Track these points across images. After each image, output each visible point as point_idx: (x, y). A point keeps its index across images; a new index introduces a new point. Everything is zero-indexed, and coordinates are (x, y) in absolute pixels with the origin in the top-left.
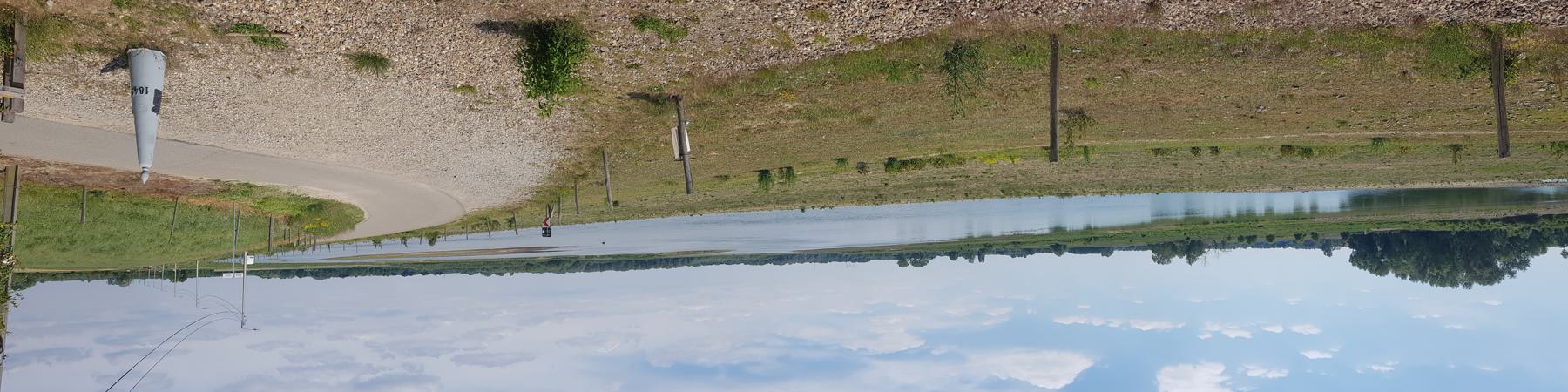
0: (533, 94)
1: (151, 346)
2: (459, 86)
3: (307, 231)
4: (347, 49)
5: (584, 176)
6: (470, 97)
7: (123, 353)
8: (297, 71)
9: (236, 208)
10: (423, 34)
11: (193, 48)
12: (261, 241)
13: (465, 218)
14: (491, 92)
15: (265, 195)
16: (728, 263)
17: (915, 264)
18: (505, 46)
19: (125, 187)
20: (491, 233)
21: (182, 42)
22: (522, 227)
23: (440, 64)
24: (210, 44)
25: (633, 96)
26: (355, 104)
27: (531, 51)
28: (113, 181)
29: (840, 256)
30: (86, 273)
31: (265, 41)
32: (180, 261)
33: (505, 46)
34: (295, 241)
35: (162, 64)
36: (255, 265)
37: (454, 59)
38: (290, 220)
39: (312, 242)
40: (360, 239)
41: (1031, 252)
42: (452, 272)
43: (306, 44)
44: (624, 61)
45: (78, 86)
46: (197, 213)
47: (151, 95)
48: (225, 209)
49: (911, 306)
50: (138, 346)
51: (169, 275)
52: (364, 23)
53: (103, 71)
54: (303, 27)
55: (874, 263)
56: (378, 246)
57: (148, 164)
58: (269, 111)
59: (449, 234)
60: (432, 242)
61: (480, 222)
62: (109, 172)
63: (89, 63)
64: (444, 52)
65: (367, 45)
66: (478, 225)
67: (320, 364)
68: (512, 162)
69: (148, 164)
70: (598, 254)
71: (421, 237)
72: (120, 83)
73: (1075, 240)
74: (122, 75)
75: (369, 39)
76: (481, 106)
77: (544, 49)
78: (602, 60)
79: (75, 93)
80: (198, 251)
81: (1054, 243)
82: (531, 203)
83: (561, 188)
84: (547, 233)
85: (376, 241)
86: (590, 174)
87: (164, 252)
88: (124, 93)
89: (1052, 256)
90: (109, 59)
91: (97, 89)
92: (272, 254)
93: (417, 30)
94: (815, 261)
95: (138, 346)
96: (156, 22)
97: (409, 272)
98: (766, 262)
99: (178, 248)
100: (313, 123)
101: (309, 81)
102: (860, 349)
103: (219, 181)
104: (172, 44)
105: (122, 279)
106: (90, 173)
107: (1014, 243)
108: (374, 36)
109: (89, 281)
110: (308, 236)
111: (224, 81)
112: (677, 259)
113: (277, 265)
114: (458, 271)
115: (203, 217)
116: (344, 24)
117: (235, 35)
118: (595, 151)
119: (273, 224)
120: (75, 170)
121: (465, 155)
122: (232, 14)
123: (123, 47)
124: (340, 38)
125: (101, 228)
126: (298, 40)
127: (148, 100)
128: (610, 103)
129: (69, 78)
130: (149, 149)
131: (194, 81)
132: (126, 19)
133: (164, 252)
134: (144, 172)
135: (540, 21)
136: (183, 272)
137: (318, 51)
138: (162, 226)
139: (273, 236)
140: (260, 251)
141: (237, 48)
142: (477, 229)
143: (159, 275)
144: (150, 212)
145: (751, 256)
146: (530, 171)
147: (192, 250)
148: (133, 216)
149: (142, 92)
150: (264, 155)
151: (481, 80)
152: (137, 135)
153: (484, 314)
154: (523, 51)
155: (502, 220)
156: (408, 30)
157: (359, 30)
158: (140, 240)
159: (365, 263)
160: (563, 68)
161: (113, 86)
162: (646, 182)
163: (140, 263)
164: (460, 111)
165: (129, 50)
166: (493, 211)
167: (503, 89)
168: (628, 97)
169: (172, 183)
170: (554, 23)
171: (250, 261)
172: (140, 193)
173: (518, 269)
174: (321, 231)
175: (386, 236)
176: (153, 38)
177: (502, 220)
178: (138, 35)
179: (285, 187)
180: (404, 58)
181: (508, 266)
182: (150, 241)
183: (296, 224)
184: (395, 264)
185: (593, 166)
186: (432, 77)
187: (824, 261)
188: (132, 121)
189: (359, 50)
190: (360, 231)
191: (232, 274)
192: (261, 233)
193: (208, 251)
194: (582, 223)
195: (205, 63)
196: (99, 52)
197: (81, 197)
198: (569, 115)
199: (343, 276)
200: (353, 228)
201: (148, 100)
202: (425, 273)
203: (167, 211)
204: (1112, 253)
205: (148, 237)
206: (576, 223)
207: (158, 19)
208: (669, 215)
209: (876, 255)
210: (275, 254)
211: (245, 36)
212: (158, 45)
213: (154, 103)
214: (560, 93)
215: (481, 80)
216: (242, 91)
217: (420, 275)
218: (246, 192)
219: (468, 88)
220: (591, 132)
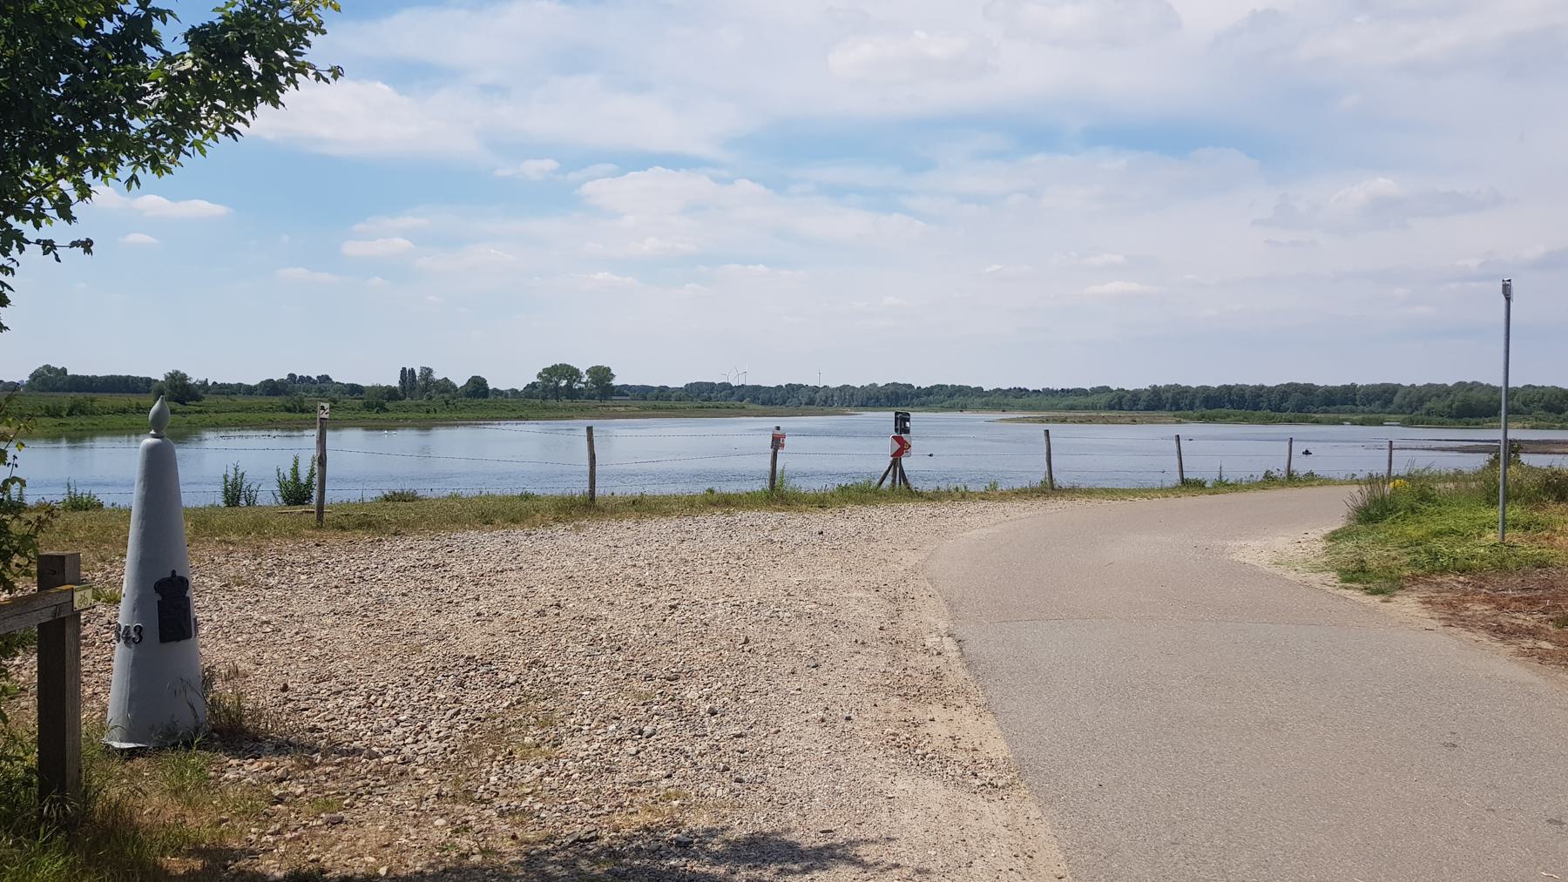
16: (1021, 392)
17: (571, 373)
29: (754, 400)
41: (271, 388)
49: (600, 276)
55: (677, 381)
70: (1347, 429)
73: (124, 411)
81: (192, 406)
89: (195, 376)
94: (816, 389)
98: (930, 391)
102: (730, 182)
107: (302, 411)
145: (963, 408)
187: (793, 389)
204: (34, 376)
209: (668, 398)
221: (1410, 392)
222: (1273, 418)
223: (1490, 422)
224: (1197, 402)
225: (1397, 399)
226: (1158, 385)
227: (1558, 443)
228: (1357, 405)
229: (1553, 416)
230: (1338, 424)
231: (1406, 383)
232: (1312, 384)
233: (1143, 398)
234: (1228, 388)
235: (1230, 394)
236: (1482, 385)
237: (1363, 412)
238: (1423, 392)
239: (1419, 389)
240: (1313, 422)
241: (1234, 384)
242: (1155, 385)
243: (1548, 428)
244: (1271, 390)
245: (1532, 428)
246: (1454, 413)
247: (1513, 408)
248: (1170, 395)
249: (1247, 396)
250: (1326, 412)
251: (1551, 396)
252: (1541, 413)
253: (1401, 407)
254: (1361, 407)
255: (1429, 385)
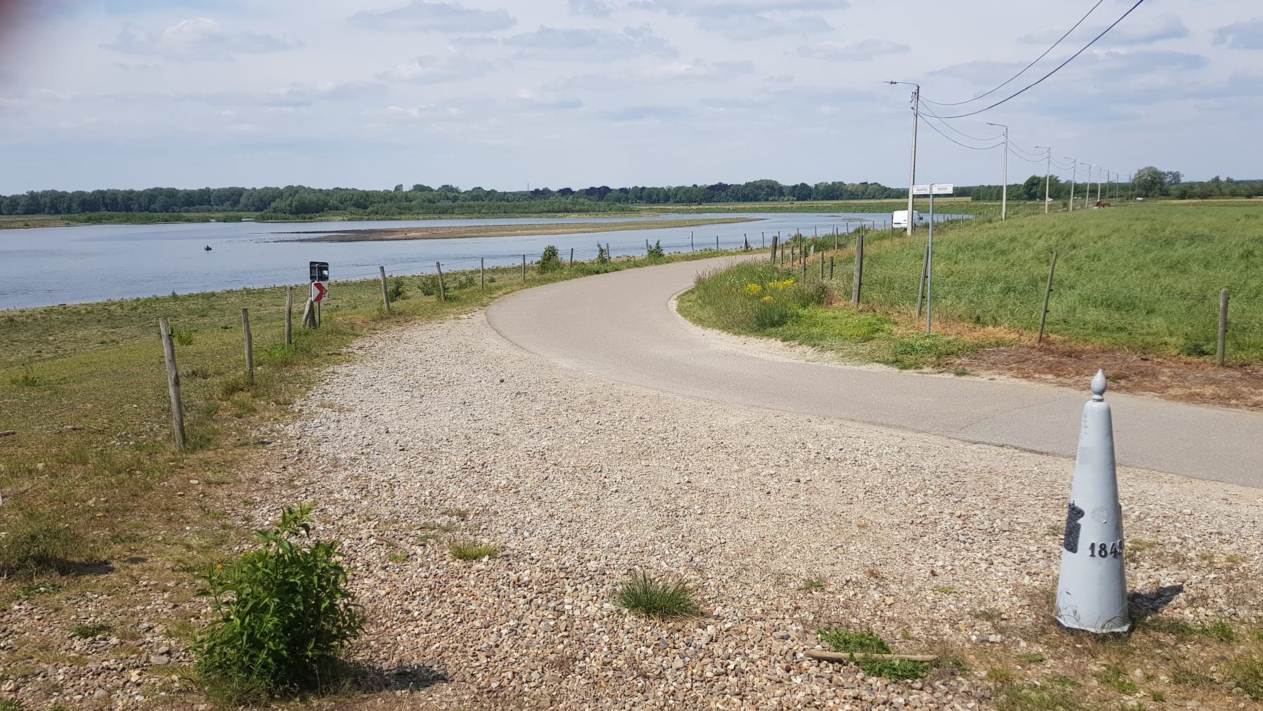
0: (321, 553)
1: (1096, 51)
2: (485, 559)
3: (788, 274)
4: (704, 628)
5: (231, 390)
6: (463, 537)
7: (1150, 39)
8: (802, 585)
9: (925, 322)
10: (552, 657)
11: (1001, 631)
12: (879, 256)
13: (485, 300)
14: (419, 551)
15: (868, 347)
18: (384, 644)
19: (1143, 364)
20: (437, 272)
21: (1023, 644)
22: (376, 282)
23: (522, 601)
24: (969, 640)
25: (103, 567)
26: (690, 520)
27: (325, 639)
28: (1165, 376)
30: (1223, 195)
31: (861, 644)
32: (1039, 218)
33: (384, 644)
34: (813, 256)
35: (1062, 601)
36: (891, 209)
37: (491, 611)
38: (821, 297)
39: (779, 253)
40: (687, 258)
42: (514, 194)
43: (782, 638)
44: (114, 640)
45: (1229, 559)
46: (1001, 312)
47: (1084, 541)
48: (946, 319)
50: (1121, 50)
51: (1060, 191)
52: (669, 677)
53: (1179, 589)
54: (788, 670)
56: (654, 245)
57: (1093, 408)
58: (857, 508)
59: (517, 269)
60: (551, 253)
61: (456, 293)
62: (1171, 391)
63: (1205, 605)
64: (511, 623)
65: (665, 634)
66: (462, 286)
67: (767, 15)
68: (386, 412)
69: (1093, 408)
70: (213, 225)
71: (572, 264)
72: (1147, 565)
74: (1141, 580)
75: (660, 647)
76: (443, 521)
77: (296, 645)
78: (169, 635)
79: (1234, 546)
80: (1002, 239)
82: (353, 332)
83: (286, 363)
84: (318, 270)
85: (656, 255)
86: (218, 393)
87: (1070, 234)
88: (1138, 546)
90: (1166, 613)
91: (1192, 554)
92: (858, 231)
93: (564, 665)
95: (1121, 50)
96: (1073, 684)
97: (596, 197)
99: (1041, 244)
100: (772, 484)
101: (778, 565)
103: (957, 374)
104: (1043, 639)
105: (1153, 183)
106: (1209, 390)
108: (650, 651)
109: (1217, 179)
110: (788, 266)
111: (943, 567)
112: (27, 212)
113: (847, 209)
114: (504, 197)
115: (991, 303)
116: (709, 674)
117: (919, 657)
118: (204, 443)
119: (855, 289)
120: (1238, 396)
121: (479, 424)
122: (925, 696)
123: (1138, 636)
124: (717, 648)
125: (1189, 283)
126: (798, 646)
127: (1091, 531)
128: (161, 546)
129: (1244, 576)
130: (1090, 438)
131: (1003, 569)
132: (1130, 689)
133: (1070, 234)
134: (1101, 393)
135: (303, 700)
136: (1032, 197)
137: (759, 624)
138: (1072, 287)
139: (855, 267)
140: (882, 237)
141: (916, 631)
142: (463, 278)
143: (1080, 190)
144: (1094, 315)
146: (350, 396)
147: (1013, 239)
148: (1127, 306)
149: (1103, 547)
150: (870, 422)
151: (440, 572)
152: (1113, 464)
153: (453, 111)
154: (345, 637)
155: (415, 297)
156: (582, 664)
157: (679, 663)
158: (1115, 260)
159: (677, 211)
160: (254, 608)
161: (1160, 560)
162: (91, 384)
163: (1115, 215)
164: (485, 509)
165: (1126, 628)
166: (431, 315)
167: (395, 558)
168: (115, 564)
169: (1050, 369)
170: (272, 698)
171: (901, 218)
172: (1112, 351)
173: (386, 197)
174: (763, 275)
175: (637, 264)
176: (1079, 653)
177: (415, 297)
178: (1108, 658)
179: (830, 362)
180: (592, 609)
181: (405, 204)
182: (1096, 257)
183: (810, 289)
184: (623, 210)
185: (211, 412)
186: (538, 575)
188: (1123, 492)
189: (679, 625)
190: (685, 276)
191: (935, 191)
192: (879, 272)
193: (980, 237)
194: (249, 292)
195: (980, 604)
196: (1186, 625)
197: (1229, 343)
198: (256, 514)
199: (721, 187)
200: (700, 281)
201: (1091, 531)
202: (566, 192)
203: (1061, 316)
205: (1099, 266)
206: (261, 292)
207: (1069, 689)
208: (49, 311)
210: (851, 230)
211: (901, 653)
212: (1068, 639)
213: (1078, 527)
214: (262, 557)
215: (440, 572)
216: (909, 547)
217: (575, 189)
218: (905, 352)
219: (467, 555)
220: (209, 483)
221: (253, 194)
222: (152, 218)
223: (320, 216)
224: (75, 206)
225: (243, 200)
226: (35, 191)
227: (386, 231)
228: (212, 205)
229: (361, 211)
230: (206, 221)
231: (249, 187)
232: (174, 189)
233: (22, 203)
234: (102, 193)
235: (104, 198)
236: (304, 188)
237: (217, 210)
238: (262, 194)
239: (259, 191)
240: (186, 221)
241: (106, 189)
242: (32, 192)
243: (360, 220)
244: (140, 194)
245: (349, 220)
246: (293, 210)
247: (334, 206)
248: (47, 200)
249: (119, 200)
250: (187, 211)
251: (358, 196)
252: (353, 209)
253: (246, 206)
254: (215, 207)
255: (267, 188)
